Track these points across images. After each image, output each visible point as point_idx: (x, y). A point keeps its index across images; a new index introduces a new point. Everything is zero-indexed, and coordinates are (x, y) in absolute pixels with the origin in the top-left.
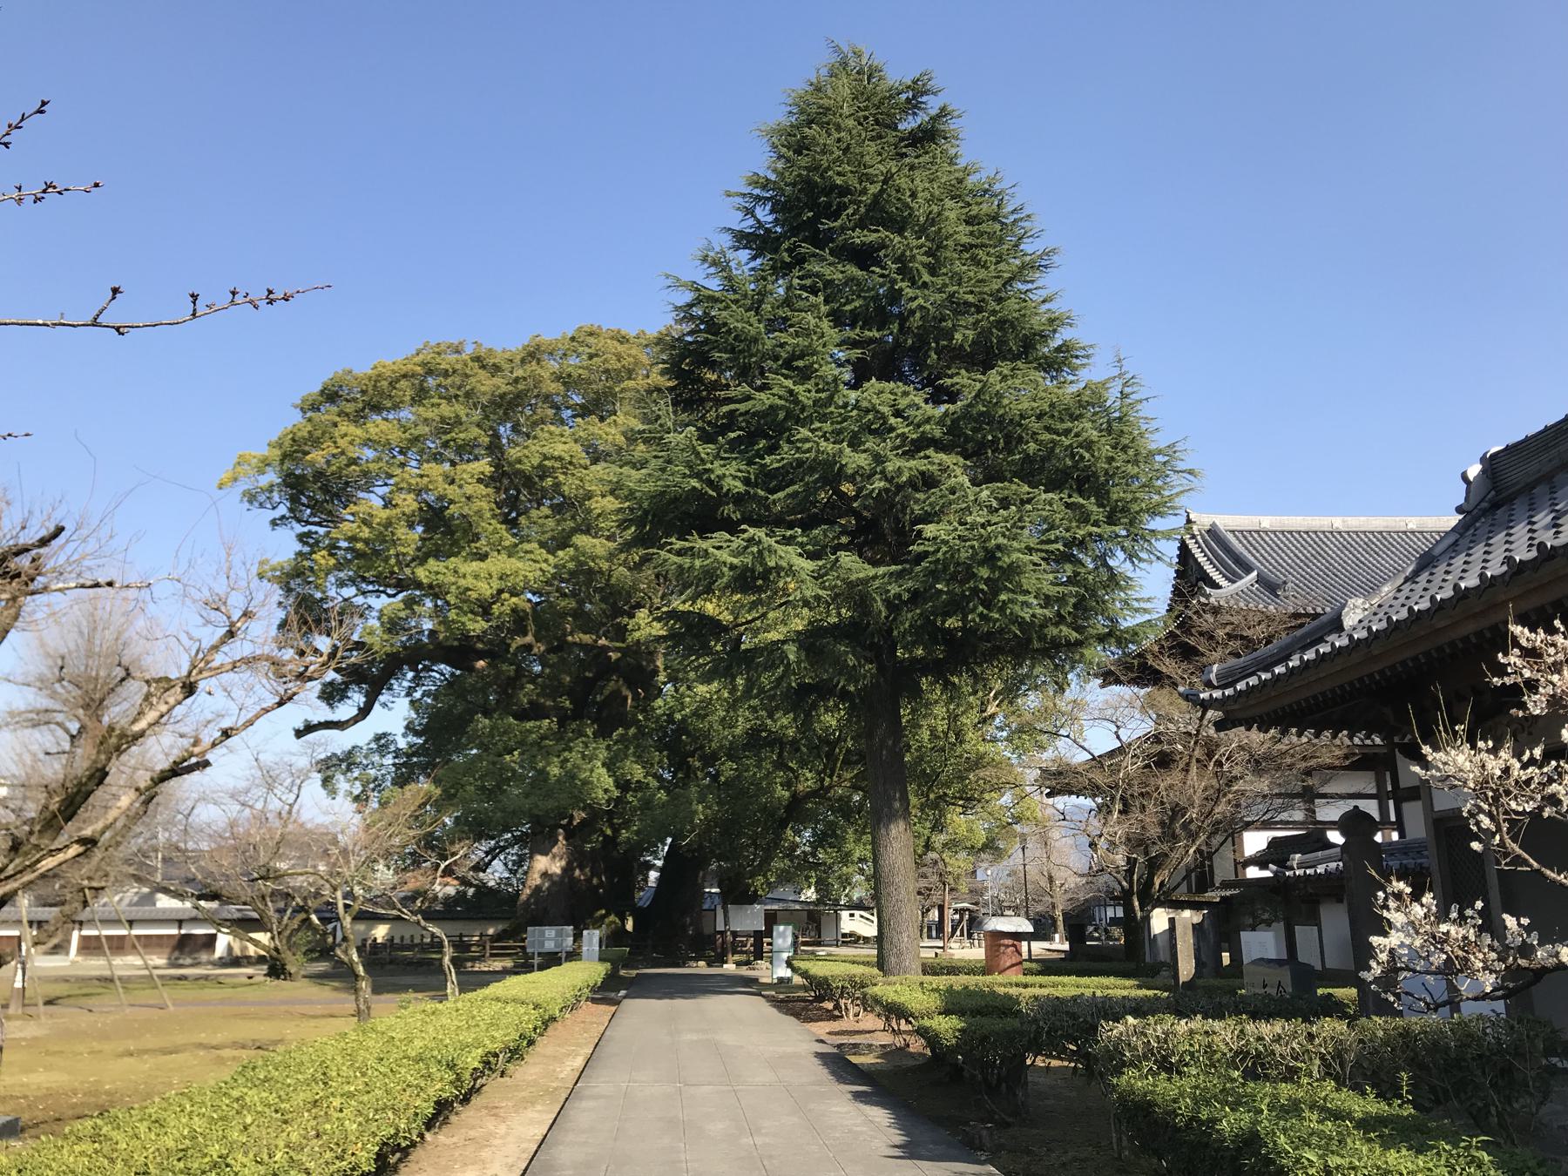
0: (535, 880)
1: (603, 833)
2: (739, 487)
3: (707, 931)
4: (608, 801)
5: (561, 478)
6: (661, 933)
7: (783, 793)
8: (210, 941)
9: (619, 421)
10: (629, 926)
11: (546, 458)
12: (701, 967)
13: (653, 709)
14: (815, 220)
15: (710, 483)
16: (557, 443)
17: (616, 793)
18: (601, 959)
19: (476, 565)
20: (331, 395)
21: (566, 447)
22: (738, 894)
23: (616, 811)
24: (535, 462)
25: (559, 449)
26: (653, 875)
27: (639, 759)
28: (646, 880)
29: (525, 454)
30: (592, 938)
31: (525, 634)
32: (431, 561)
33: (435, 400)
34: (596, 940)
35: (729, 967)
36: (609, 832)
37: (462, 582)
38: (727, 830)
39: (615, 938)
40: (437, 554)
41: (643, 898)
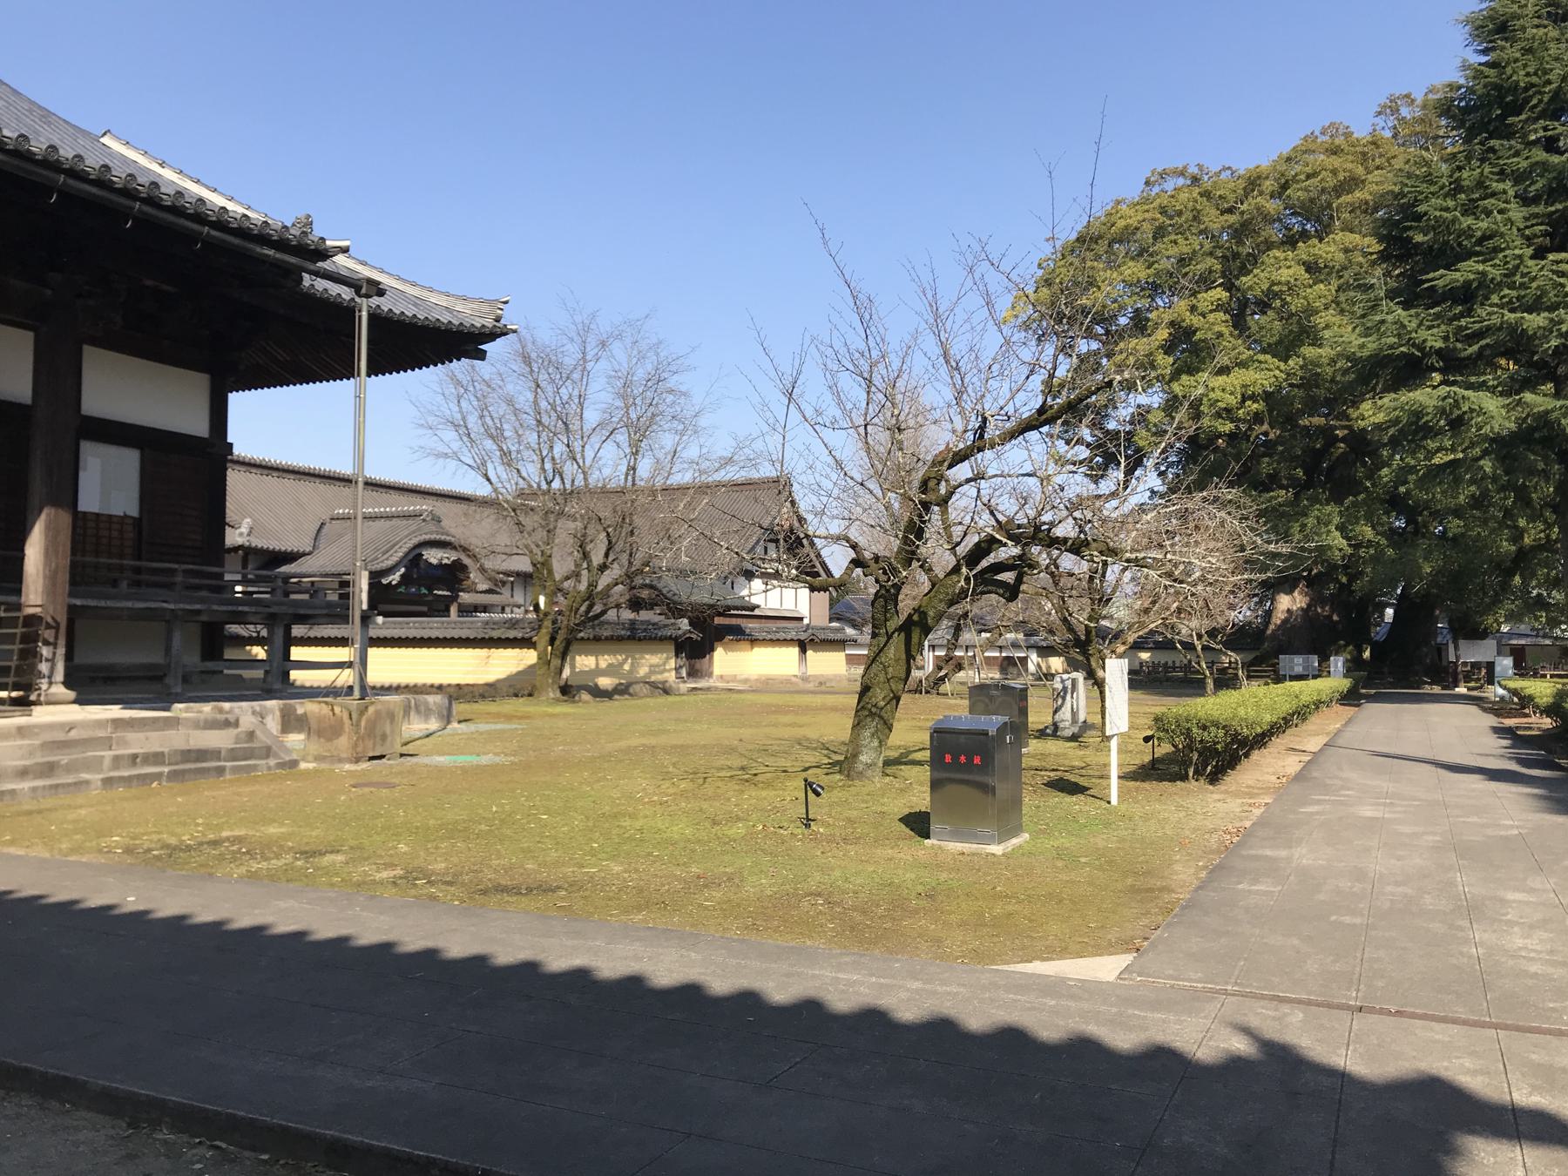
0: (1279, 617)
1: (1337, 581)
2: (1439, 344)
3: (1444, 663)
4: (1343, 558)
5: (1288, 299)
6: (1400, 664)
7: (1507, 547)
8: (1024, 660)
9: (1338, 238)
10: (1367, 654)
11: (1273, 284)
12: (1437, 690)
13: (1380, 477)
14: (1503, 117)
15: (1414, 345)
16: (1281, 268)
17: (1350, 551)
18: (1345, 676)
19: (1221, 380)
20: (1086, 240)
21: (1291, 272)
22: (1471, 630)
23: (1351, 566)
24: (1265, 287)
25: (1285, 275)
26: (1390, 612)
27: (1369, 518)
28: (1382, 615)
29: (1254, 282)
30: (1338, 663)
31: (1262, 424)
32: (1184, 377)
33: (1173, 237)
34: (1340, 664)
35: (1461, 690)
36: (1344, 580)
37: (1212, 395)
38: (1454, 582)
39: (1354, 666)
40: (1191, 371)
41: (1379, 633)
